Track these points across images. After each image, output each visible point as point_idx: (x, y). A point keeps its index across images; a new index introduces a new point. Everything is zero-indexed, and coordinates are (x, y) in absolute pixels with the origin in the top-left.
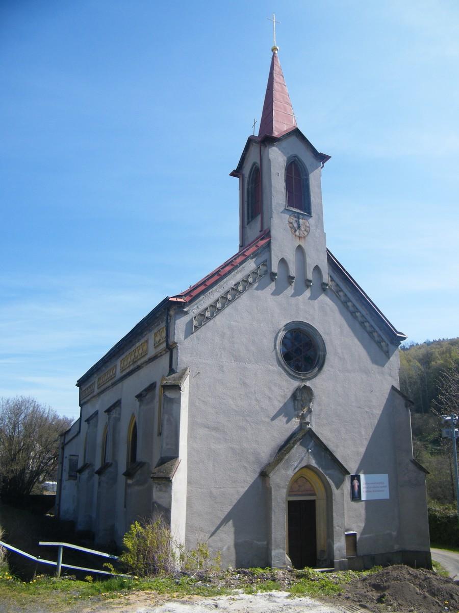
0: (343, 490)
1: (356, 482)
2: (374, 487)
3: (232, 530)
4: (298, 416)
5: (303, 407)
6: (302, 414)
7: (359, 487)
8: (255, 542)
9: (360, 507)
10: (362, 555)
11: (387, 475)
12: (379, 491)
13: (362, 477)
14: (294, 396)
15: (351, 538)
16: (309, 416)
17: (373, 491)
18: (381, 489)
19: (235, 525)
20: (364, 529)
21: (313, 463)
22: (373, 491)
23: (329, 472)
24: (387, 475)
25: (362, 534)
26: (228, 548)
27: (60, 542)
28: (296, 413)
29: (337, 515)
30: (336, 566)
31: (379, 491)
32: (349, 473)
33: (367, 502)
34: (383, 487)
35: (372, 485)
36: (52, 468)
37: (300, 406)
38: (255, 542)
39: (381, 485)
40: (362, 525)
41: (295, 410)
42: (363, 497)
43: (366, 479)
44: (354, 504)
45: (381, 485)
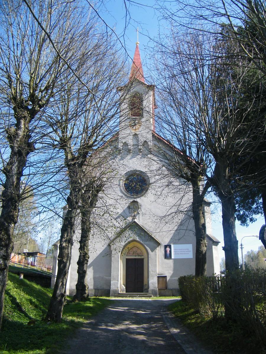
0: (156, 252)
1: (168, 249)
2: (181, 252)
3: (92, 271)
4: (131, 216)
5: (134, 211)
6: (134, 215)
7: (170, 251)
8: (105, 277)
9: (170, 262)
10: (172, 288)
11: (192, 245)
12: (185, 254)
13: (172, 246)
14: (129, 207)
15: (162, 278)
16: (138, 216)
17: (181, 254)
18: (186, 253)
19: (93, 269)
20: (173, 274)
21: (137, 239)
22: (181, 254)
23: (147, 243)
24: (192, 245)
25: (171, 277)
26: (91, 279)
27: (132, 300)
28: (130, 214)
29: (152, 266)
30: (150, 292)
31: (185, 254)
32: (158, 244)
33: (175, 260)
34: (188, 251)
35: (180, 251)
36: (253, 287)
37: (132, 211)
38: (105, 277)
39: (187, 250)
40: (172, 272)
41: (130, 213)
42: (173, 257)
43: (174, 247)
44: (167, 261)
45: (187, 250)
